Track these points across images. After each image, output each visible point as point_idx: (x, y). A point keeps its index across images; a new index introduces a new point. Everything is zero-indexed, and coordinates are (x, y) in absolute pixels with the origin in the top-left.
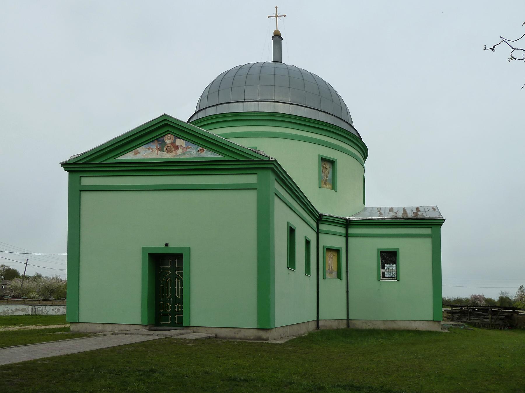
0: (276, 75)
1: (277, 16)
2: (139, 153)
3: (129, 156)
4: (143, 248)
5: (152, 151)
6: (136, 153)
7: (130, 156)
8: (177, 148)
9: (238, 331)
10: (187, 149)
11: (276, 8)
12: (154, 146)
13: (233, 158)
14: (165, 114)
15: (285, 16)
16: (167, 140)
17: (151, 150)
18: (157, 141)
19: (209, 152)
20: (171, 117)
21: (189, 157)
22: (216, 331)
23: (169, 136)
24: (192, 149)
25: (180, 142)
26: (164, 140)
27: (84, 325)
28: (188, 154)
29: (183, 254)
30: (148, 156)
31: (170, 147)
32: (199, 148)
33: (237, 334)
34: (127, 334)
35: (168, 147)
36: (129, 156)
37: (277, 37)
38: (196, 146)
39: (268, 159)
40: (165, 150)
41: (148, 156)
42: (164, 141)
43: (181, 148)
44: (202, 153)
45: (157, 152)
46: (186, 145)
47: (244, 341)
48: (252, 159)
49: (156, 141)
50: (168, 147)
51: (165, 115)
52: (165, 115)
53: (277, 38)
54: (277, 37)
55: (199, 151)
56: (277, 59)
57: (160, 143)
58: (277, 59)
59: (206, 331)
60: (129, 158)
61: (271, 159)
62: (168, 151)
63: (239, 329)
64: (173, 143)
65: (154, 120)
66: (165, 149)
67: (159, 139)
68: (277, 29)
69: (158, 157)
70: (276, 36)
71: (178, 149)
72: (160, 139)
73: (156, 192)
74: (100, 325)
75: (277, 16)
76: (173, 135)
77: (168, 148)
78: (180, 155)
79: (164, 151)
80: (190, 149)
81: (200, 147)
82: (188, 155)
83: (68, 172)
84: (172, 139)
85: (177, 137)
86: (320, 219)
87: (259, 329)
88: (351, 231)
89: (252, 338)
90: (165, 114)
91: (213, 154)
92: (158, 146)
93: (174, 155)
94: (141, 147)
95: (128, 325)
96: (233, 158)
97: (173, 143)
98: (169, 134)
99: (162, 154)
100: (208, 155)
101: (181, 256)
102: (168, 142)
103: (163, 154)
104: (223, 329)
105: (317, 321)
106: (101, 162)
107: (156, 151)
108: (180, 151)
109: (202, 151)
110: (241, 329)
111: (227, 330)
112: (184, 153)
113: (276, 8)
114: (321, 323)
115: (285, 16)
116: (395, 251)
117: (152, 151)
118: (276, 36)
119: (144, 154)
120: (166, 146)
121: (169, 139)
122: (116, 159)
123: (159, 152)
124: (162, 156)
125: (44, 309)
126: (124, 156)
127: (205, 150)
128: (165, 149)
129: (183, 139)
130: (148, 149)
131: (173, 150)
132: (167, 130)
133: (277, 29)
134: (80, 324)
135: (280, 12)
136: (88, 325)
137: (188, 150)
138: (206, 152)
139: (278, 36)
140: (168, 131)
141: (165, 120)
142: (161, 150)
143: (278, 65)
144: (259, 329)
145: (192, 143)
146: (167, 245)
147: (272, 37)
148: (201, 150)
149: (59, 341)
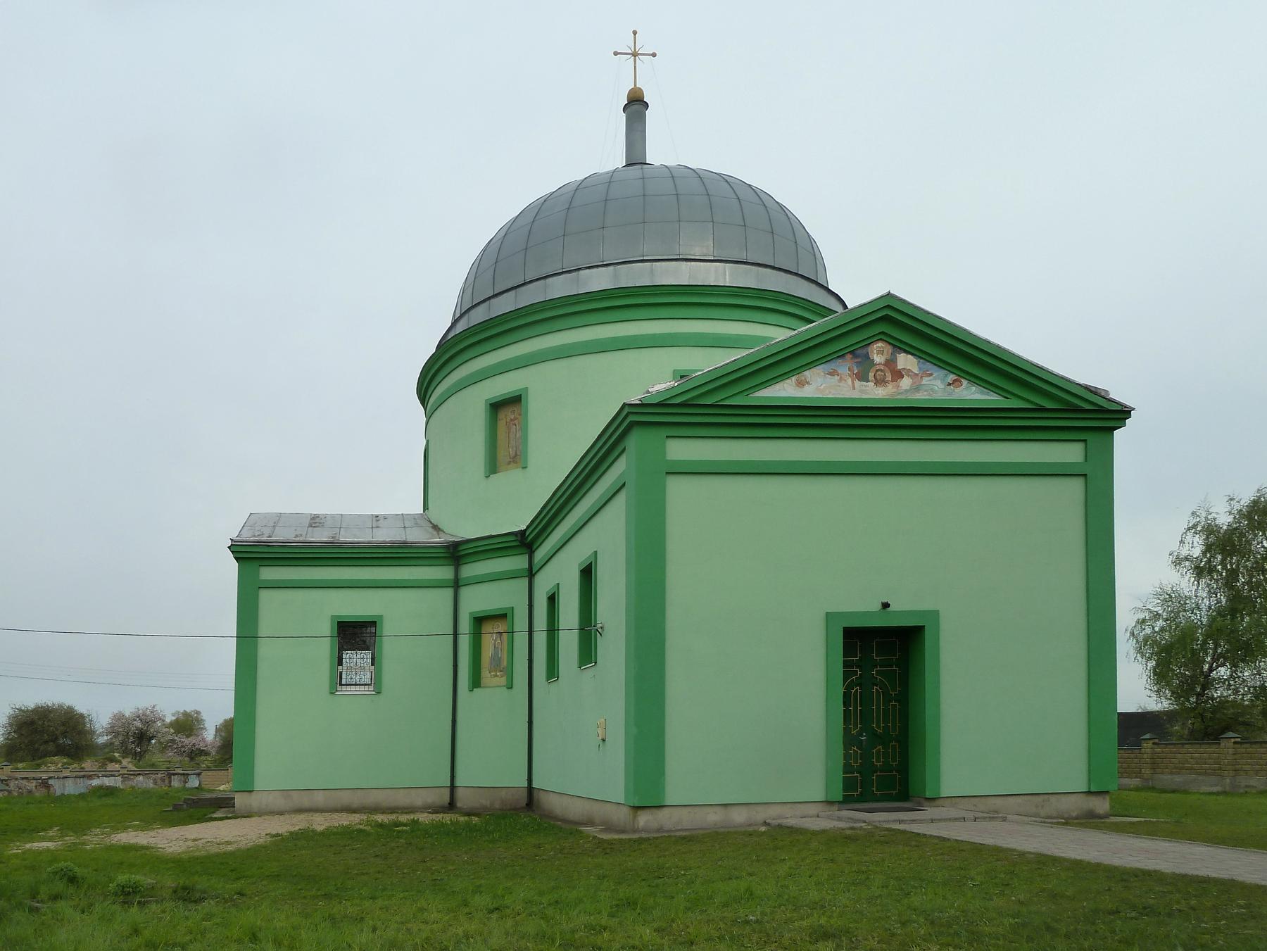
0: (712, 195)
1: (635, 54)
2: (808, 383)
4: (935, 614)
5: (841, 379)
6: (801, 384)
7: (784, 391)
8: (898, 375)
9: (1043, 801)
10: (922, 377)
11: (635, 33)
12: (845, 367)
13: (1028, 401)
14: (889, 292)
15: (654, 55)
16: (875, 355)
17: (837, 378)
18: (851, 356)
19: (974, 388)
20: (904, 302)
21: (927, 397)
22: (995, 804)
23: (880, 344)
24: (935, 379)
25: (905, 361)
26: (868, 353)
27: (677, 813)
30: (830, 392)
32: (952, 377)
33: (1042, 806)
34: (903, 821)
35: (877, 371)
36: (785, 390)
37: (636, 104)
38: (943, 372)
39: (1119, 408)
41: (830, 392)
42: (867, 356)
43: (908, 375)
44: (957, 390)
45: (853, 383)
46: (920, 369)
48: (1040, 406)
49: (849, 356)
52: (889, 294)
53: (635, 107)
54: (636, 104)
55: (950, 384)
56: (636, 157)
57: (860, 362)
58: (636, 157)
59: (975, 805)
60: (783, 394)
61: (1125, 407)
62: (880, 382)
63: (1046, 797)
64: (891, 363)
65: (862, 306)
66: (871, 375)
67: (859, 355)
68: (635, 85)
69: (856, 394)
70: (634, 101)
72: (859, 352)
73: (857, 479)
74: (717, 809)
75: (635, 54)
76: (890, 343)
78: (906, 391)
79: (868, 381)
80: (931, 378)
81: (955, 374)
82: (925, 393)
84: (888, 352)
85: (900, 347)
86: (525, 542)
87: (1089, 793)
88: (469, 570)
89: (1074, 814)
90: (889, 292)
91: (982, 393)
92: (855, 368)
94: (812, 370)
95: (789, 806)
96: (1028, 401)
97: (891, 363)
98: (881, 339)
99: (864, 388)
100: (970, 394)
101: (918, 630)
102: (878, 359)
104: (1010, 799)
105: (453, 788)
106: (684, 401)
107: (850, 379)
108: (906, 383)
109: (956, 383)
110: (1050, 796)
111: (1019, 800)
112: (916, 388)
113: (635, 33)
114: (460, 794)
115: (654, 55)
116: (332, 620)
117: (841, 379)
118: (634, 101)
119: (822, 387)
120: (873, 370)
121: (881, 352)
122: (751, 395)
123: (857, 383)
124: (862, 391)
126: (770, 389)
127: (965, 382)
129: (912, 354)
130: (831, 374)
132: (881, 331)
133: (635, 85)
134: (666, 811)
135: (644, 45)
136: (685, 811)
137: (925, 381)
138: (966, 388)
139: (637, 101)
140: (883, 333)
141: (888, 306)
142: (862, 377)
143: (635, 171)
144: (1089, 793)
145: (935, 365)
146: (886, 605)
148: (955, 381)
149: (1141, 838)
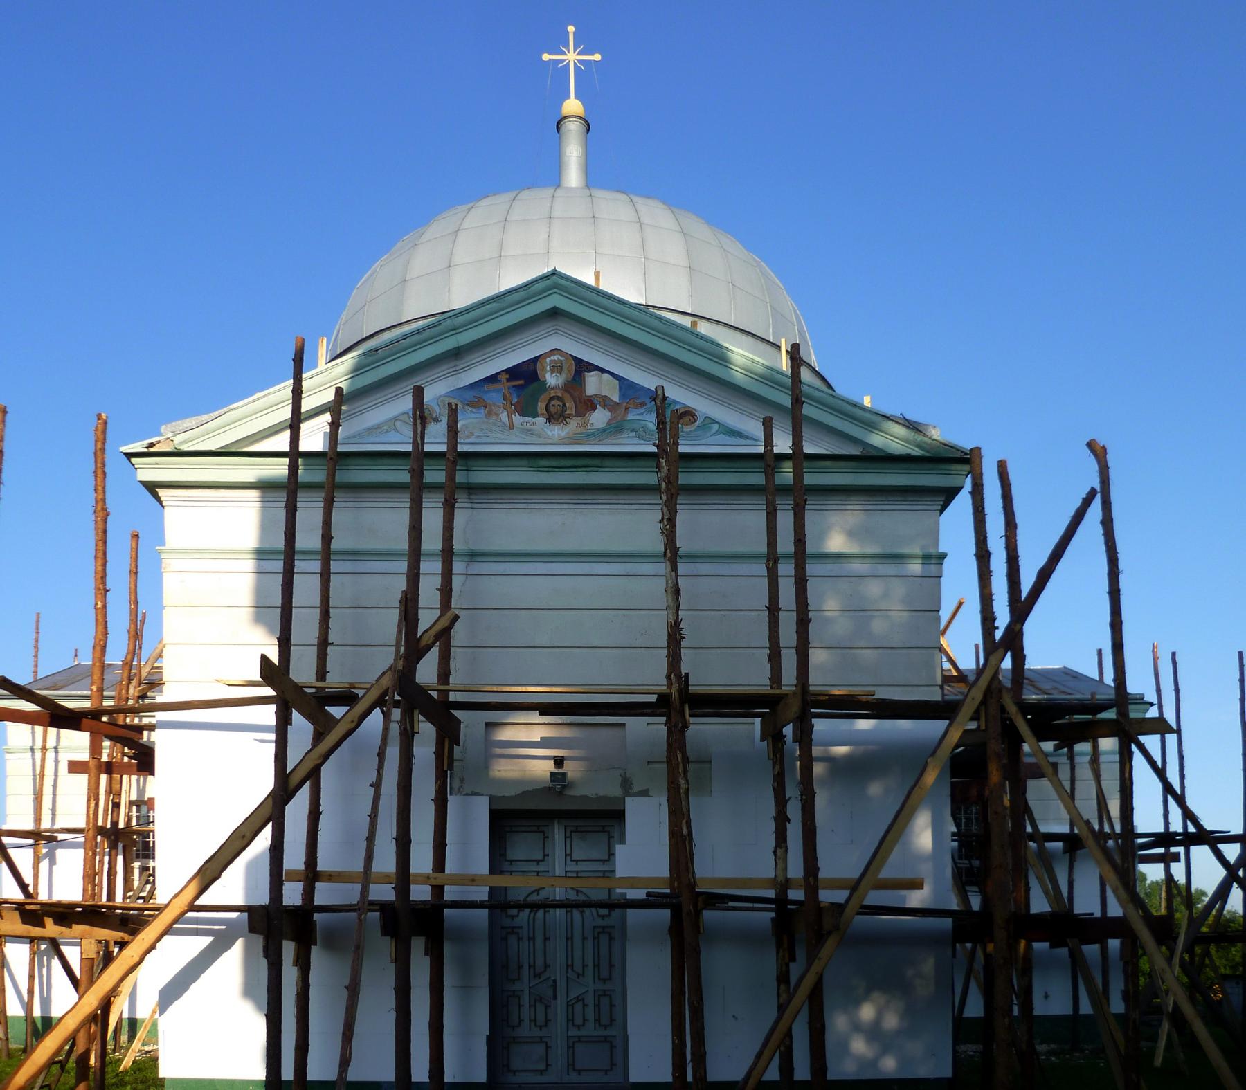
3: (396, 430)
5: (490, 414)
8: (589, 405)
10: (627, 409)
26: (535, 371)
28: (633, 430)
29: (69, 772)
31: (559, 398)
36: (396, 430)
40: (539, 410)
43: (604, 406)
45: (510, 418)
47: (559, 1047)
50: (552, 399)
51: (554, 274)
66: (541, 406)
71: (594, 408)
77: (552, 403)
79: (536, 415)
83: (302, 426)
93: (579, 430)
103: (534, 427)
108: (599, 418)
123: (517, 419)
125: (109, 1047)
128: (541, 406)
131: (571, 409)
142: (527, 409)
147: (304, 339)
